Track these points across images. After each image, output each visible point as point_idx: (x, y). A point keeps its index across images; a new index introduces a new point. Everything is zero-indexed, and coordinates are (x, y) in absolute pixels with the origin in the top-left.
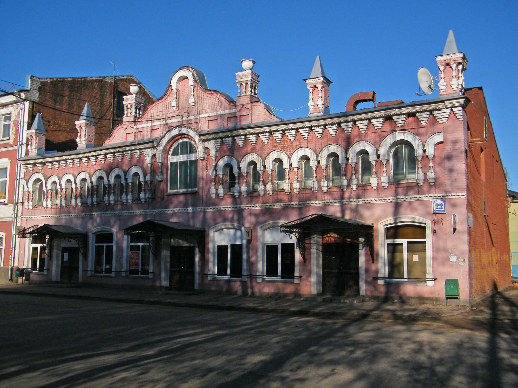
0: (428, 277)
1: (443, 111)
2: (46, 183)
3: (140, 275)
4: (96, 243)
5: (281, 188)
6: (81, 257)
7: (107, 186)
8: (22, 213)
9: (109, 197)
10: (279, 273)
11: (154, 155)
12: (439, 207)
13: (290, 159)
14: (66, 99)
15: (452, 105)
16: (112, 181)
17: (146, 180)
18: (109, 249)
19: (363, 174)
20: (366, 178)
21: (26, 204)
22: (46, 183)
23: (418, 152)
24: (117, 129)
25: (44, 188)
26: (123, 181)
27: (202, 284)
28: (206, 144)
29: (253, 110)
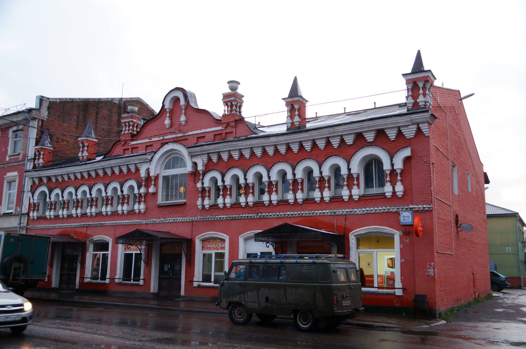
0: (396, 287)
1: (410, 127)
2: (50, 195)
3: (132, 282)
4: (93, 251)
5: (311, 197)
6: (79, 265)
7: (75, 201)
8: (27, 223)
9: (203, 201)
10: (213, 280)
11: (148, 170)
12: (406, 218)
13: (245, 176)
14: (75, 117)
15: (418, 121)
16: (109, 194)
17: (204, 186)
18: (105, 257)
19: (336, 188)
20: (311, 193)
21: (31, 214)
22: (50, 195)
23: (387, 167)
24: (118, 146)
25: (48, 200)
26: (119, 193)
27: (82, 283)
28: (195, 160)
29: (238, 129)
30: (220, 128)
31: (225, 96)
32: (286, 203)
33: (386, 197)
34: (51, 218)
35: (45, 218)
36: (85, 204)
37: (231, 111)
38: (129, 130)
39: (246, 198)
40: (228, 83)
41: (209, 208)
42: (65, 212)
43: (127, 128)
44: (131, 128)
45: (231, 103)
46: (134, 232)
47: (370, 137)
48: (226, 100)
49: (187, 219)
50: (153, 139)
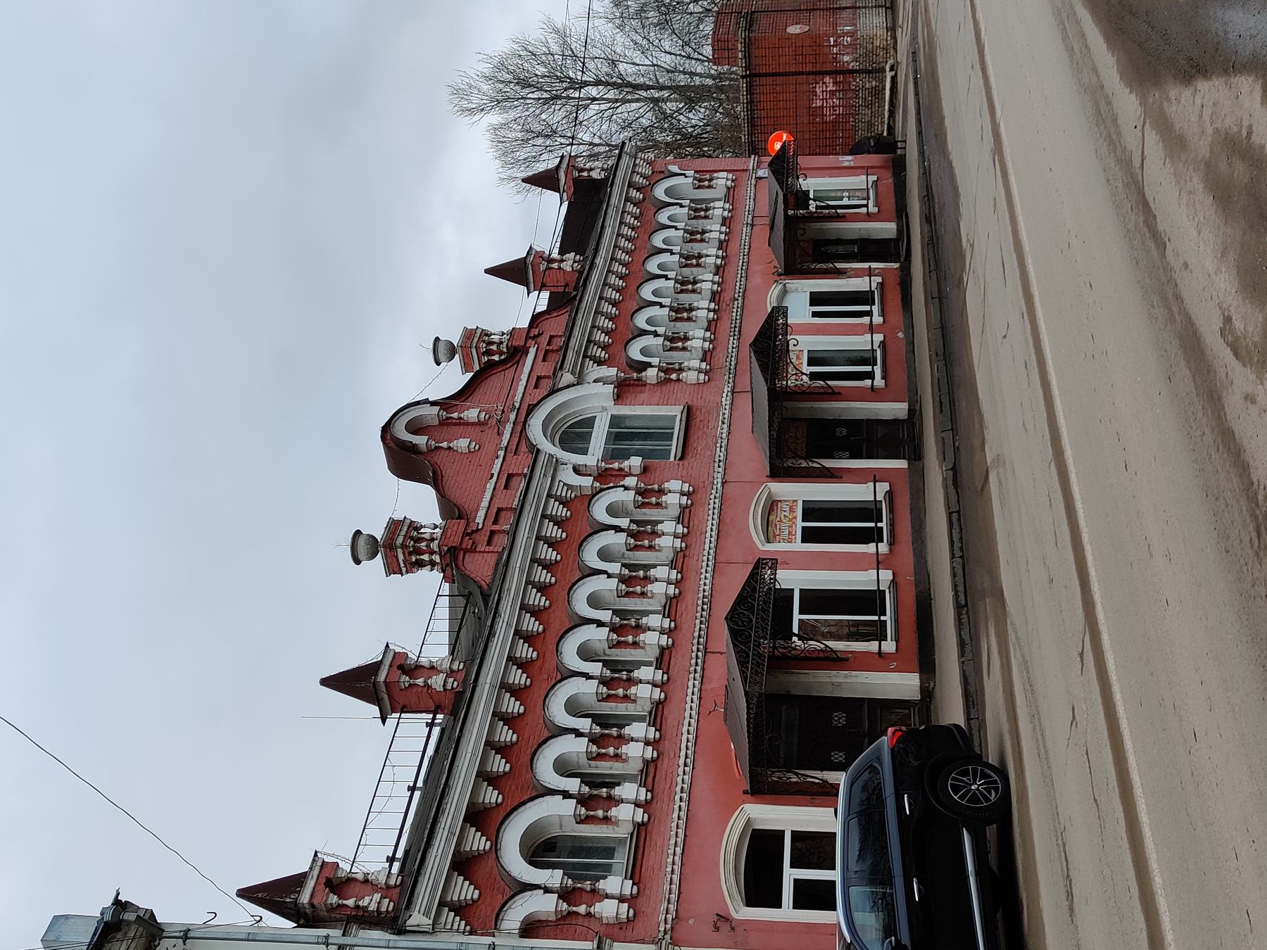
11: (576, 470)
30: (532, 351)
31: (392, 568)
32: (713, 324)
33: (653, 760)
34: (677, 583)
35: (659, 705)
36: (642, 557)
37: (433, 564)
38: (432, 553)
39: (607, 896)
40: (438, 364)
41: (659, 730)
42: (645, 673)
43: (426, 557)
44: (494, 347)
45: (483, 354)
46: (734, 634)
47: (477, 842)
48: (404, 570)
49: (726, 401)
50: (496, 470)
